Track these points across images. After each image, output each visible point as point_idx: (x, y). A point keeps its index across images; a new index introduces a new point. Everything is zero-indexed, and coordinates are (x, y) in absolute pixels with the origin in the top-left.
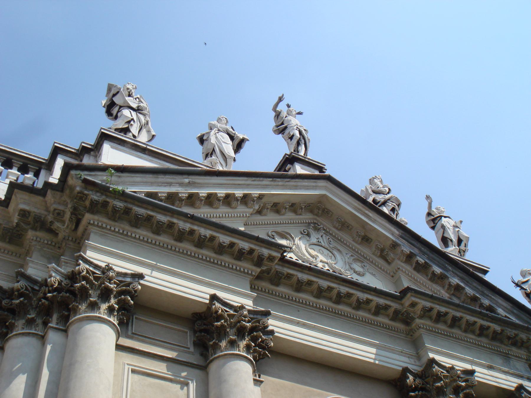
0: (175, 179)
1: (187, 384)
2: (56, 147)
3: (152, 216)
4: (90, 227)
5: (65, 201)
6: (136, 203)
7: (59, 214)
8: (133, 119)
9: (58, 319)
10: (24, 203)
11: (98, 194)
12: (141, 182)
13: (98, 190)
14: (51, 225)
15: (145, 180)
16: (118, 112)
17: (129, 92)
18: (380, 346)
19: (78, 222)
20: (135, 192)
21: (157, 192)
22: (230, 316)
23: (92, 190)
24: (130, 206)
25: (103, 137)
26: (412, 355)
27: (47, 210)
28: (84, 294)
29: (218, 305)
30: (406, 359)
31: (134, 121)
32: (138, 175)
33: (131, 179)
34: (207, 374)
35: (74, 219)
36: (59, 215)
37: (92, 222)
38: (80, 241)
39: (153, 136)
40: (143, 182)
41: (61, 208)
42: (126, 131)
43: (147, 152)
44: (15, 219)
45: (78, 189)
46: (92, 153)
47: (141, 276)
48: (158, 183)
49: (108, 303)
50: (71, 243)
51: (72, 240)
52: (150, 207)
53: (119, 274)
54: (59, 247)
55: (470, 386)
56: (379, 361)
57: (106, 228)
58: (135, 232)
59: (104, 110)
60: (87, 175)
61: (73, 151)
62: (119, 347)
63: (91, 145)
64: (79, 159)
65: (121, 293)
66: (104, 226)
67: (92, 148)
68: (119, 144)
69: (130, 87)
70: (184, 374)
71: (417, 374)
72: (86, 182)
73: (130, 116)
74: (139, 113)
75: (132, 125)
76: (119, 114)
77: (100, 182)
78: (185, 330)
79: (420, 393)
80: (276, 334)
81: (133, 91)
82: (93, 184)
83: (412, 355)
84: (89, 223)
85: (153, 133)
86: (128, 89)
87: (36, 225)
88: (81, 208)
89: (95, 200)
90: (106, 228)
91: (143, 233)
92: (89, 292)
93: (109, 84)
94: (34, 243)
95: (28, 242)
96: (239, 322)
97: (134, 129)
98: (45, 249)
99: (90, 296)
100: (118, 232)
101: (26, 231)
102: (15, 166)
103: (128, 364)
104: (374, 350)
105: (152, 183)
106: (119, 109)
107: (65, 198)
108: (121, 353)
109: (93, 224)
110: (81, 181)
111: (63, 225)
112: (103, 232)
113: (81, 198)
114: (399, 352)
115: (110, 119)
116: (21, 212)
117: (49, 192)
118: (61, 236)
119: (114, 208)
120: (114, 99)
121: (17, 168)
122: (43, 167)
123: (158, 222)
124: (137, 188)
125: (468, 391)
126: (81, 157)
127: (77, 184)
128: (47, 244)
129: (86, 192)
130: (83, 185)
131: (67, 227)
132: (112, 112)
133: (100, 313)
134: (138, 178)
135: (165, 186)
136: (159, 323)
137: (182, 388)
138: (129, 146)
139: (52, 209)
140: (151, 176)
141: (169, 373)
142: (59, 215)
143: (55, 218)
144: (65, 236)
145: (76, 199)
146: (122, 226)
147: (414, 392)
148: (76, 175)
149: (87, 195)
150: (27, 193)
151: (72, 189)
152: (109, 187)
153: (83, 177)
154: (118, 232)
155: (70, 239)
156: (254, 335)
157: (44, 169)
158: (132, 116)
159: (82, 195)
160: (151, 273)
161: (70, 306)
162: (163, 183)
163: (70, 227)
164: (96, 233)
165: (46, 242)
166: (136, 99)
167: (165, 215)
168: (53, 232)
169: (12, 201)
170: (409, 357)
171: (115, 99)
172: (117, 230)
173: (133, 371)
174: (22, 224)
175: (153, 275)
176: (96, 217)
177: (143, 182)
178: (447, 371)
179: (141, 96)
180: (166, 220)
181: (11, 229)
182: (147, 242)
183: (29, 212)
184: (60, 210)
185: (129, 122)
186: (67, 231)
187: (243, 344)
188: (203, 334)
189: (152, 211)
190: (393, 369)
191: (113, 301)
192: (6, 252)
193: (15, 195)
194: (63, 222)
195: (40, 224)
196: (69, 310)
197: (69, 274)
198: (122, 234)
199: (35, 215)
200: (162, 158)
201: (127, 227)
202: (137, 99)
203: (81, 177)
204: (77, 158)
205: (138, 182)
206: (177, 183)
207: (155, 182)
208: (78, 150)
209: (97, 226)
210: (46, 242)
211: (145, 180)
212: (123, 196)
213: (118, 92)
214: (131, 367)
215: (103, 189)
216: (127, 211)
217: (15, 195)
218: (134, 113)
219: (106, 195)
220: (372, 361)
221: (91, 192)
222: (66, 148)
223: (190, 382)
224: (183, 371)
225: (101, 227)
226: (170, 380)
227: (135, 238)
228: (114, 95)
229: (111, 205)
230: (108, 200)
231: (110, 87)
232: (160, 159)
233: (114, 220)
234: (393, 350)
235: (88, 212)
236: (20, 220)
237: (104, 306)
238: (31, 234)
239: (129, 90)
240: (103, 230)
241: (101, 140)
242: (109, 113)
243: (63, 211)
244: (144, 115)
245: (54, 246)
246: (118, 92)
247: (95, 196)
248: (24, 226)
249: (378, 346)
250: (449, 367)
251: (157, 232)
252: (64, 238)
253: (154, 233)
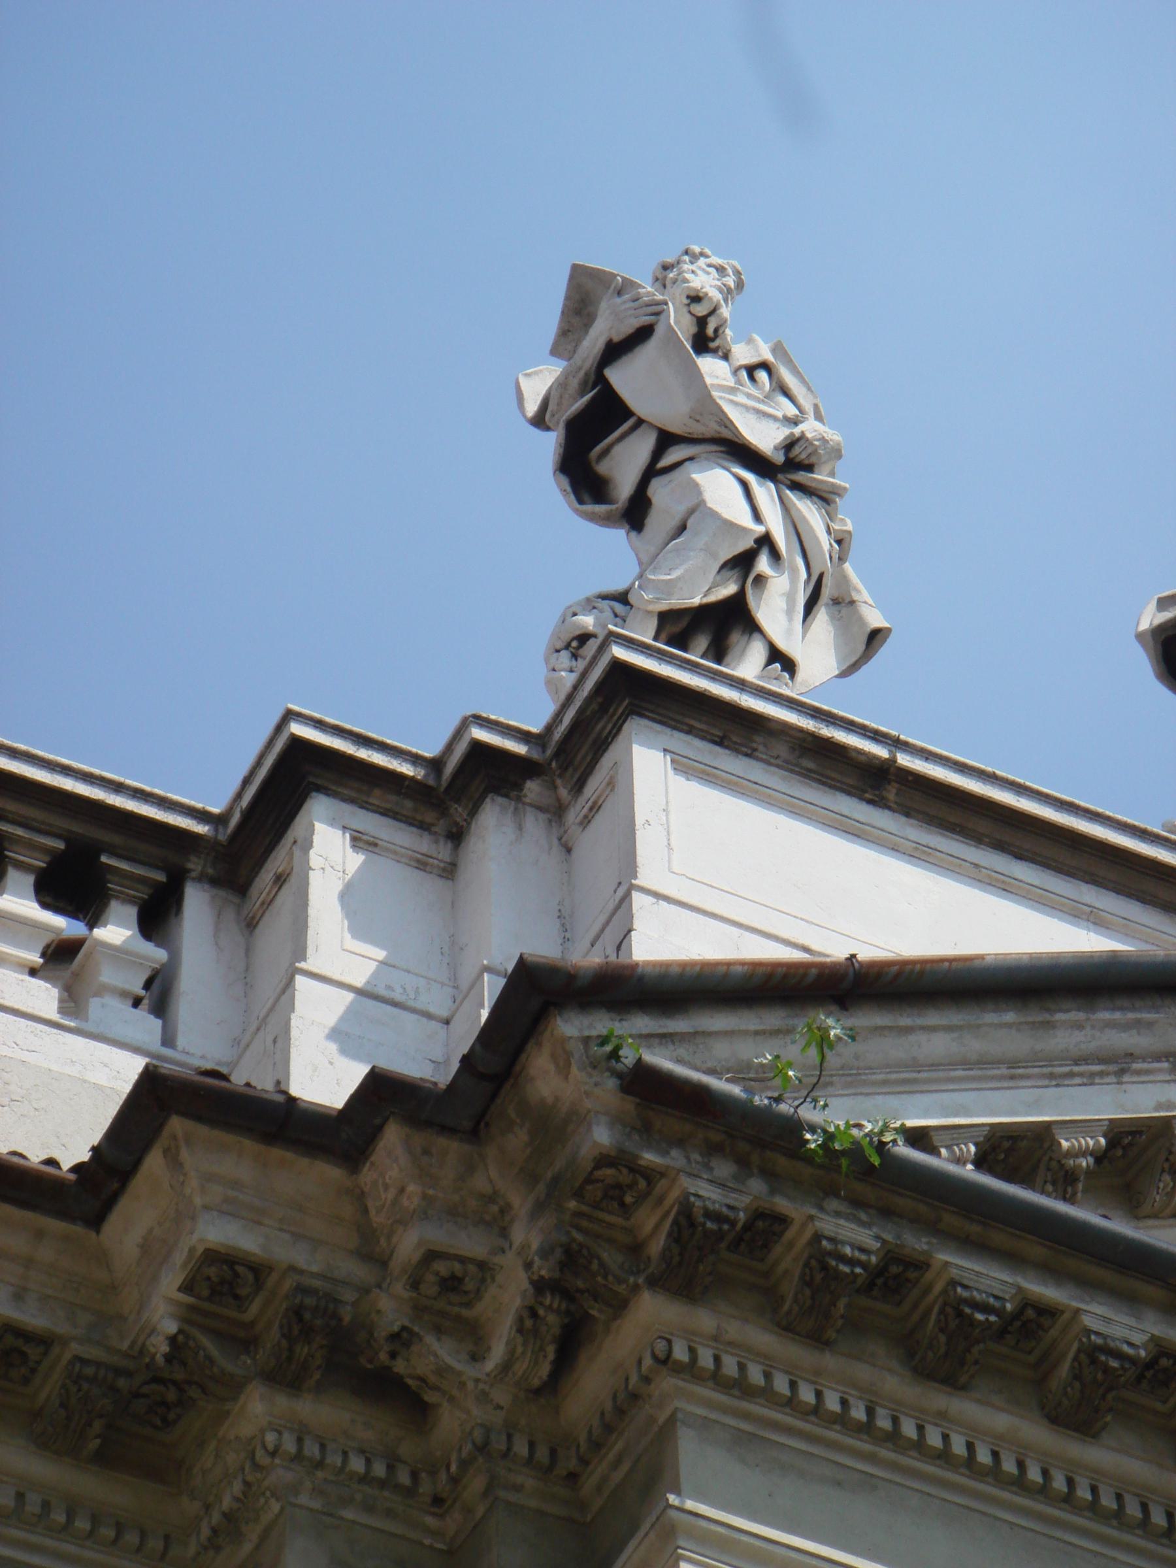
0: (1150, 1025)
2: (297, 743)
3: (1048, 1312)
4: (667, 1383)
5: (491, 1198)
6: (950, 1220)
7: (451, 1284)
8: (765, 541)
10: (229, 1209)
11: (724, 1169)
12: (953, 1064)
13: (715, 1137)
14: (393, 1355)
15: (974, 1046)
16: (651, 472)
17: (702, 322)
19: (571, 1343)
20: (919, 1138)
21: (1049, 1125)
23: (680, 1142)
24: (916, 1243)
25: (619, 699)
27: (371, 1250)
31: (775, 555)
32: (933, 1017)
33: (893, 1048)
35: (552, 1318)
36: (450, 1289)
37: (680, 1353)
38: (584, 1462)
39: (875, 637)
40: (965, 1063)
41: (471, 1243)
42: (726, 623)
43: (891, 793)
44: (161, 1314)
45: (602, 1136)
46: (533, 788)
48: (1050, 1059)
50: (528, 1481)
51: (530, 1461)
52: (1036, 1250)
54: (438, 1501)
57: (766, 1393)
58: (942, 1415)
59: (549, 444)
60: (647, 1038)
61: (407, 769)
63: (524, 736)
64: (441, 827)
66: (755, 1375)
67: (536, 755)
68: (720, 742)
69: (702, 280)
72: (645, 1085)
73: (744, 519)
74: (796, 487)
75: (760, 580)
76: (659, 491)
77: (736, 1090)
81: (725, 312)
82: (694, 1102)
84: (665, 1361)
85: (875, 619)
86: (696, 298)
87: (302, 1351)
88: (611, 1258)
89: (709, 1214)
90: (766, 1393)
91: (988, 1419)
93: (576, 269)
94: (281, 1475)
95: (232, 1458)
97: (776, 609)
98: (349, 1514)
100: (842, 1420)
101: (235, 1387)
102: (21, 866)
105: (1013, 1063)
106: (658, 453)
107: (492, 1176)
109: (690, 1370)
110: (611, 1083)
111: (476, 1357)
112: (746, 1416)
113: (615, 1195)
115: (592, 518)
116: (212, 1271)
117: (393, 1136)
118: (451, 1424)
119: (822, 1261)
120: (620, 377)
121: (30, 880)
122: (195, 865)
123: (1095, 1353)
124: (933, 1105)
126: (458, 811)
127: (588, 1104)
128: (365, 1479)
129: (650, 1157)
130: (629, 1104)
131: (506, 1367)
132: (602, 468)
134: (935, 1035)
135: (1091, 1079)
138: (782, 749)
139: (408, 1245)
140: (1010, 1017)
142: (450, 1289)
143: (419, 1310)
144: (487, 1430)
145: (578, 1194)
146: (863, 1372)
148: (586, 1040)
149: (651, 1175)
150: (249, 1144)
151: (552, 1127)
152: (793, 1128)
153: (628, 1057)
154: (842, 1420)
155: (521, 1448)
157: (200, 879)
158: (757, 517)
159: (625, 1177)
162: (1077, 1062)
163: (520, 1368)
164: (705, 1424)
165: (357, 1464)
166: (751, 370)
167: (1130, 1300)
168: (408, 1401)
169: (139, 1183)
171: (624, 378)
172: (832, 1403)
174: (205, 1341)
176: (705, 1320)
177: (965, 1063)
179: (778, 349)
180: (1138, 1338)
181: (118, 1372)
182: (1019, 1483)
183: (259, 1270)
184: (463, 1260)
185: (743, 563)
186: (502, 1395)
189: (1051, 1272)
192: (82, 1524)
193: (173, 1159)
194: (474, 1337)
195: (331, 1348)
198: (867, 1428)
199: (301, 1289)
200: (983, 826)
201: (896, 1384)
202: (762, 375)
203: (614, 1055)
204: (430, 817)
205: (934, 1066)
206: (1158, 1058)
207: (1035, 1059)
208: (435, 765)
209: (716, 1378)
210: (357, 1464)
211: (974, 1046)
212: (873, 1176)
213: (643, 334)
215: (761, 1139)
216: (894, 1276)
217: (173, 1159)
218: (765, 492)
219: (769, 1174)
221: (675, 1159)
222: (363, 754)
225: (740, 1387)
227: (944, 1456)
228: (615, 351)
229: (797, 1238)
230: (782, 1204)
231: (585, 293)
232: (977, 839)
233: (818, 1339)
235: (654, 1283)
236: (189, 1316)
238: (258, 1410)
239: (701, 310)
240: (746, 1405)
241: (603, 709)
242: (582, 475)
243: (482, 1265)
244: (824, 497)
245: (410, 1492)
246: (643, 334)
247: (710, 1187)
248: (226, 1363)
251: (1079, 1417)
252: (483, 1448)
253: (1056, 1418)
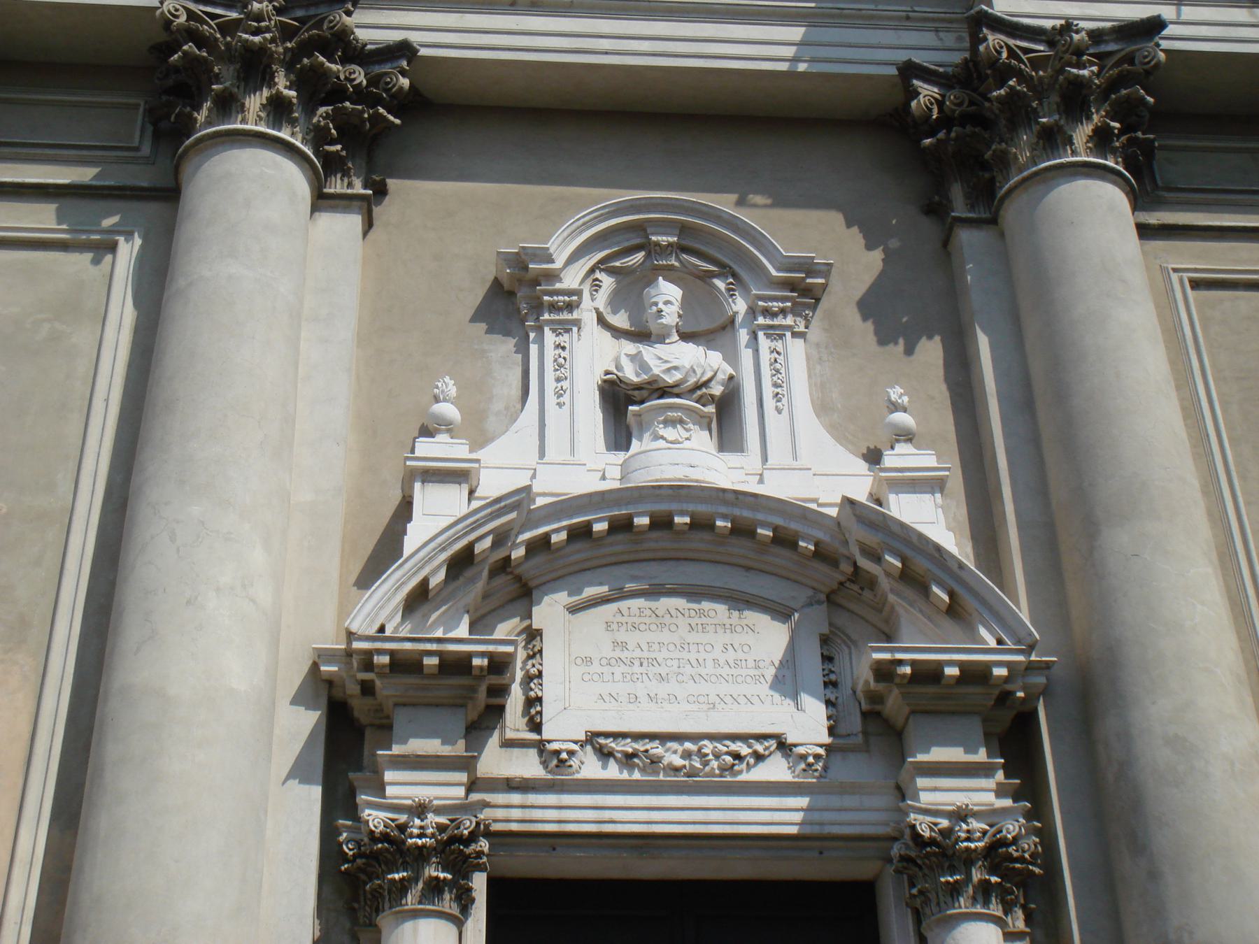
1: (112, 248)
9: (967, 196)
18: (823, 16)
22: (1036, 63)
26: (950, 21)
28: (1017, 112)
29: (993, 39)
30: (928, 38)
34: (1002, 235)
47: (1155, 26)
49: (270, 87)
53: (1096, 36)
55: (1149, 75)
56: (812, 60)
62: (1145, 231)
65: (1113, 85)
70: (107, 223)
71: (954, 76)
78: (132, 101)
79: (953, 135)
80: (423, 52)
83: (950, 21)
92: (212, 70)
96: (1061, 71)
99: (1036, 114)
103: (1175, 270)
104: (796, 33)
108: (1158, 245)
114: (899, 19)
125: (1124, 92)
133: (1074, 153)
136: (34, 97)
137: (96, 262)
141: (64, 227)
147: (932, 134)
156: (303, 67)
160: (1179, 14)
161: (988, 155)
170: (937, 30)
173: (1196, 284)
175: (1184, 17)
178: (1051, 44)
187: (1082, 133)
188: (969, 129)
190: (869, 77)
191: (282, 84)
196: (985, 166)
197: (958, 70)
214: (1186, 276)
220: (783, 67)
223: (121, 239)
224: (109, 214)
226: (62, 246)
234: (872, 17)
237: (1082, 133)
249: (815, 15)
250: (1054, 28)
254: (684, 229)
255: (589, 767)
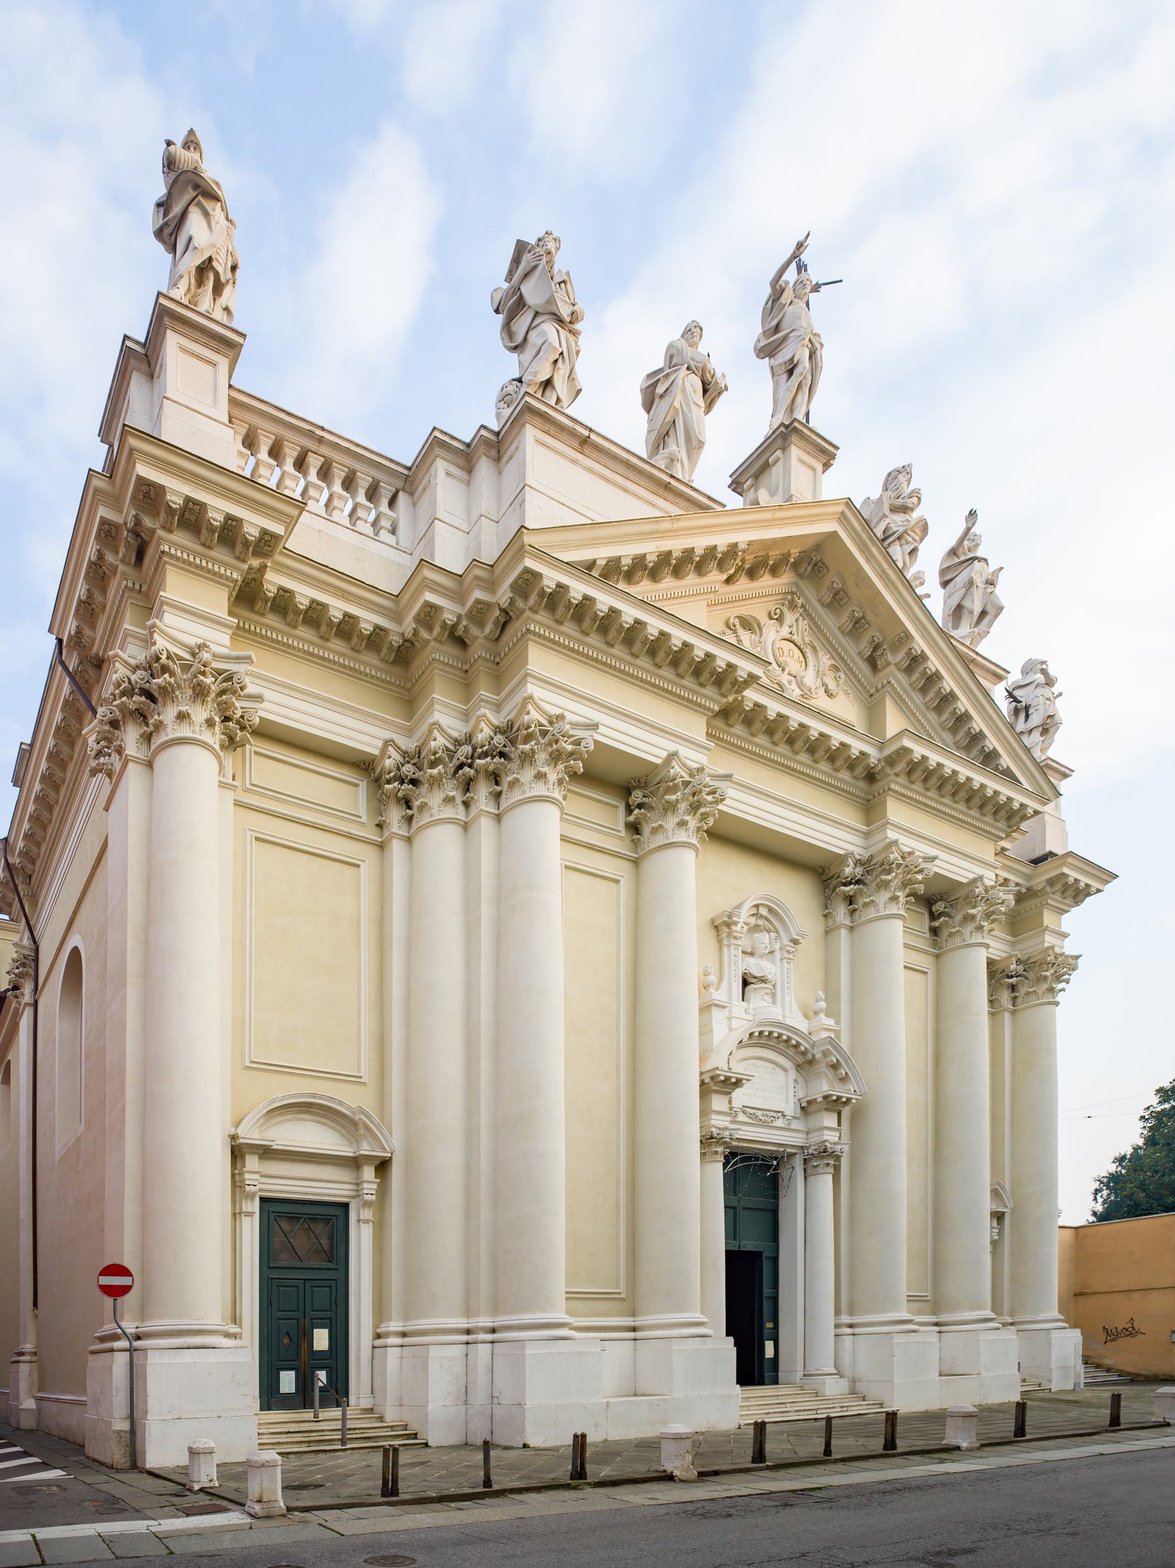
254: (770, 910)
255: (742, 1118)
